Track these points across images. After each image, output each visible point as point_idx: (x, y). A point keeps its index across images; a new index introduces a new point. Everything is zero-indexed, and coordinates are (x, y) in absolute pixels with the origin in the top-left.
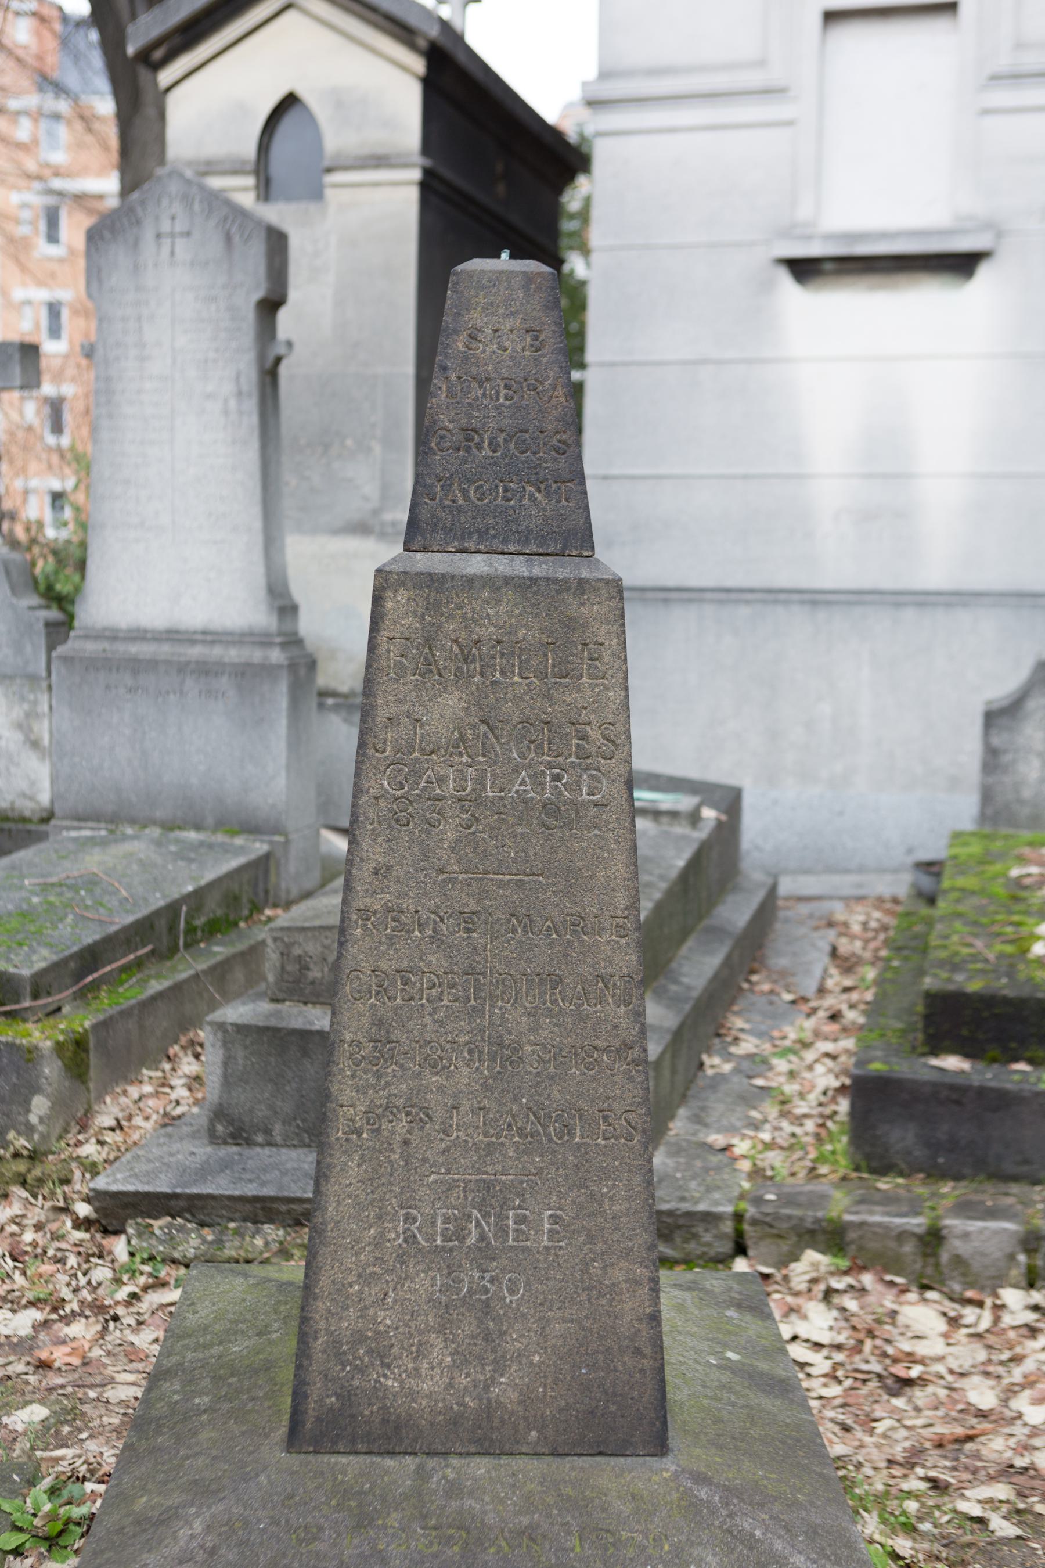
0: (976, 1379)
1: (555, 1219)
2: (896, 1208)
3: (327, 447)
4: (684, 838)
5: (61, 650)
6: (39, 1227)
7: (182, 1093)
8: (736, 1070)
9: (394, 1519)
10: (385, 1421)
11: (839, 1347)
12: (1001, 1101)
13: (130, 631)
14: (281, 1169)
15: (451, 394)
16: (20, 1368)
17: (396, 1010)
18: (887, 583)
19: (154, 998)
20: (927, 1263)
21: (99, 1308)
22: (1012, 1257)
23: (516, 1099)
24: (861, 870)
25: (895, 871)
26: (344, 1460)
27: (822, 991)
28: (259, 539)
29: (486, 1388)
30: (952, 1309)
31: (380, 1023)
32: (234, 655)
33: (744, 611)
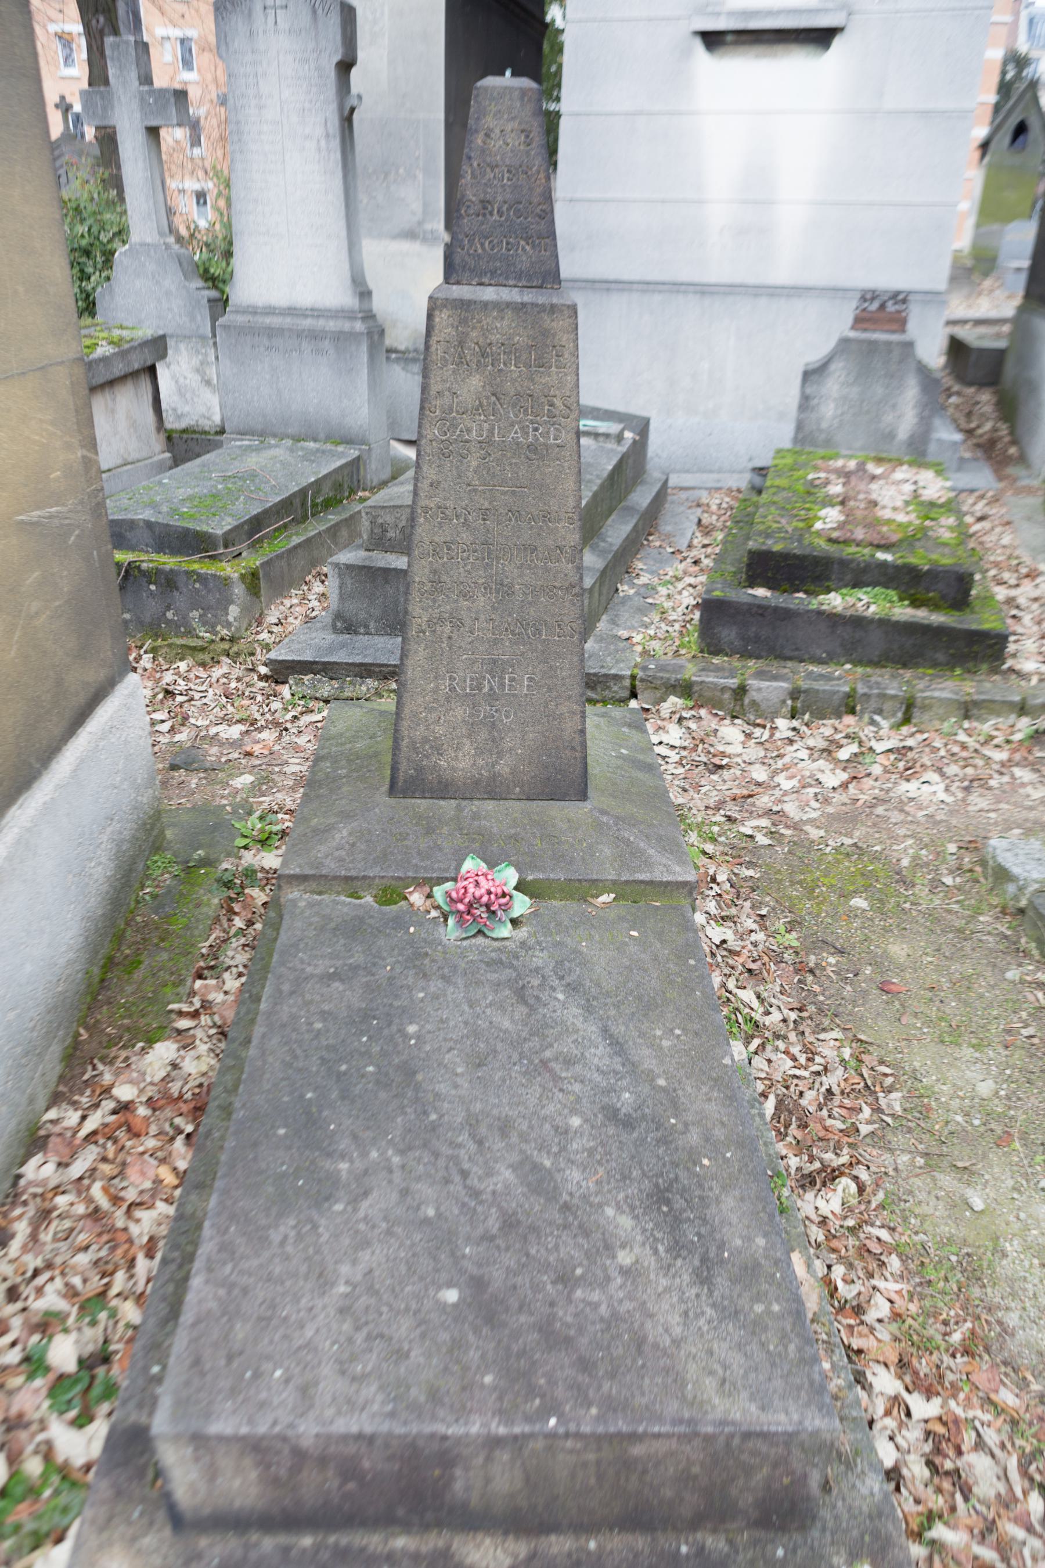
0: (757, 766)
1: (530, 679)
2: (721, 674)
3: (387, 175)
4: (612, 450)
5: (221, 321)
6: (239, 680)
7: (315, 603)
8: (637, 593)
9: (445, 830)
10: (440, 782)
11: (685, 748)
12: (785, 615)
13: (265, 308)
14: (380, 648)
15: (474, 176)
16: (236, 755)
17: (443, 564)
18: (751, 280)
19: (295, 547)
20: (737, 704)
21: (278, 724)
22: (784, 702)
23: (510, 615)
24: (720, 471)
25: (741, 472)
26: (419, 801)
27: (690, 546)
28: (345, 244)
29: (493, 766)
30: (748, 729)
31: (435, 572)
32: (332, 325)
33: (657, 298)
